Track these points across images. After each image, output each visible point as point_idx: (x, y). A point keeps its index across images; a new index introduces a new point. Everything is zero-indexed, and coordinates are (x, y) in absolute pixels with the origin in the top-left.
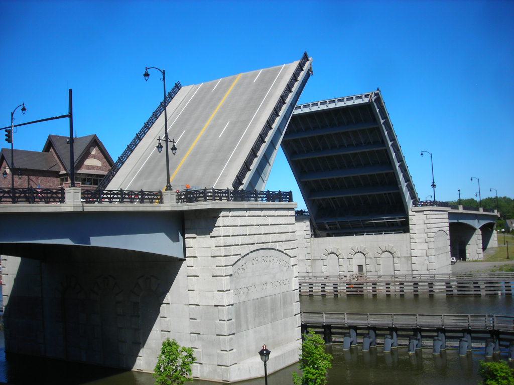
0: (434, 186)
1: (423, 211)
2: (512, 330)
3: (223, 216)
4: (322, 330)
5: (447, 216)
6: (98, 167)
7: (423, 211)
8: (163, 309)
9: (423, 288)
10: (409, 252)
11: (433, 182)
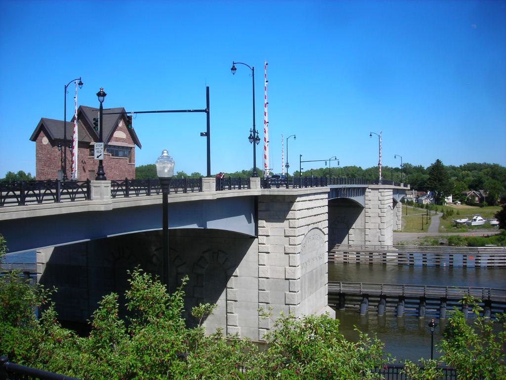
0: (254, 139)
1: (378, 189)
2: (504, 301)
3: (298, 202)
4: (338, 297)
5: (392, 193)
6: (123, 139)
7: (378, 189)
8: (232, 282)
9: (377, 258)
10: (363, 224)
11: (254, 131)
